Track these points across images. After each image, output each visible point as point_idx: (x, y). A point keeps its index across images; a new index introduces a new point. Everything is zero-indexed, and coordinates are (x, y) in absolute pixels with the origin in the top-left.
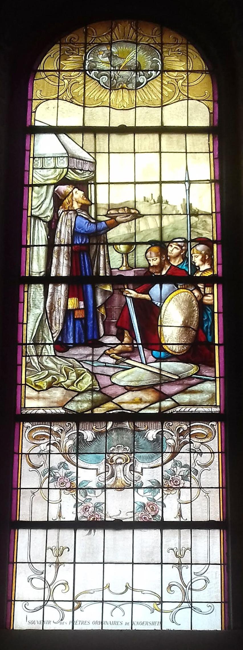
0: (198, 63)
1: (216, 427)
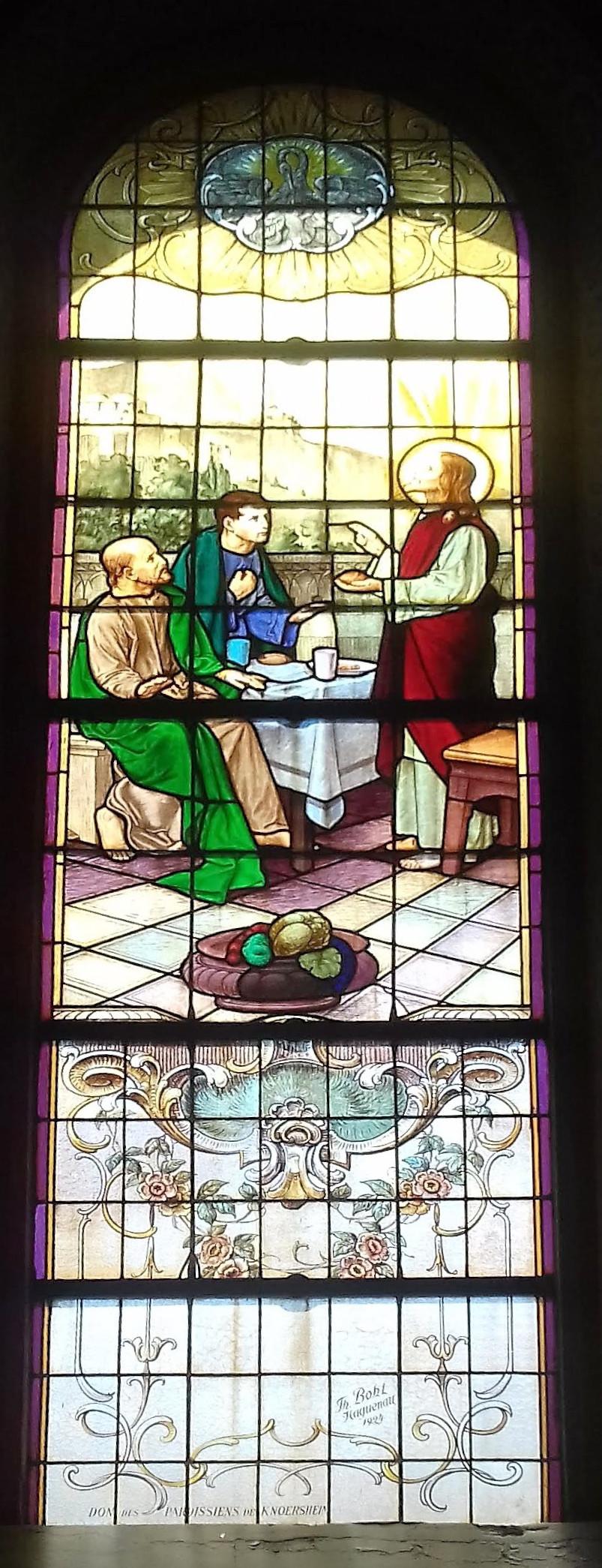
0: (478, 188)
1: (525, 1056)
